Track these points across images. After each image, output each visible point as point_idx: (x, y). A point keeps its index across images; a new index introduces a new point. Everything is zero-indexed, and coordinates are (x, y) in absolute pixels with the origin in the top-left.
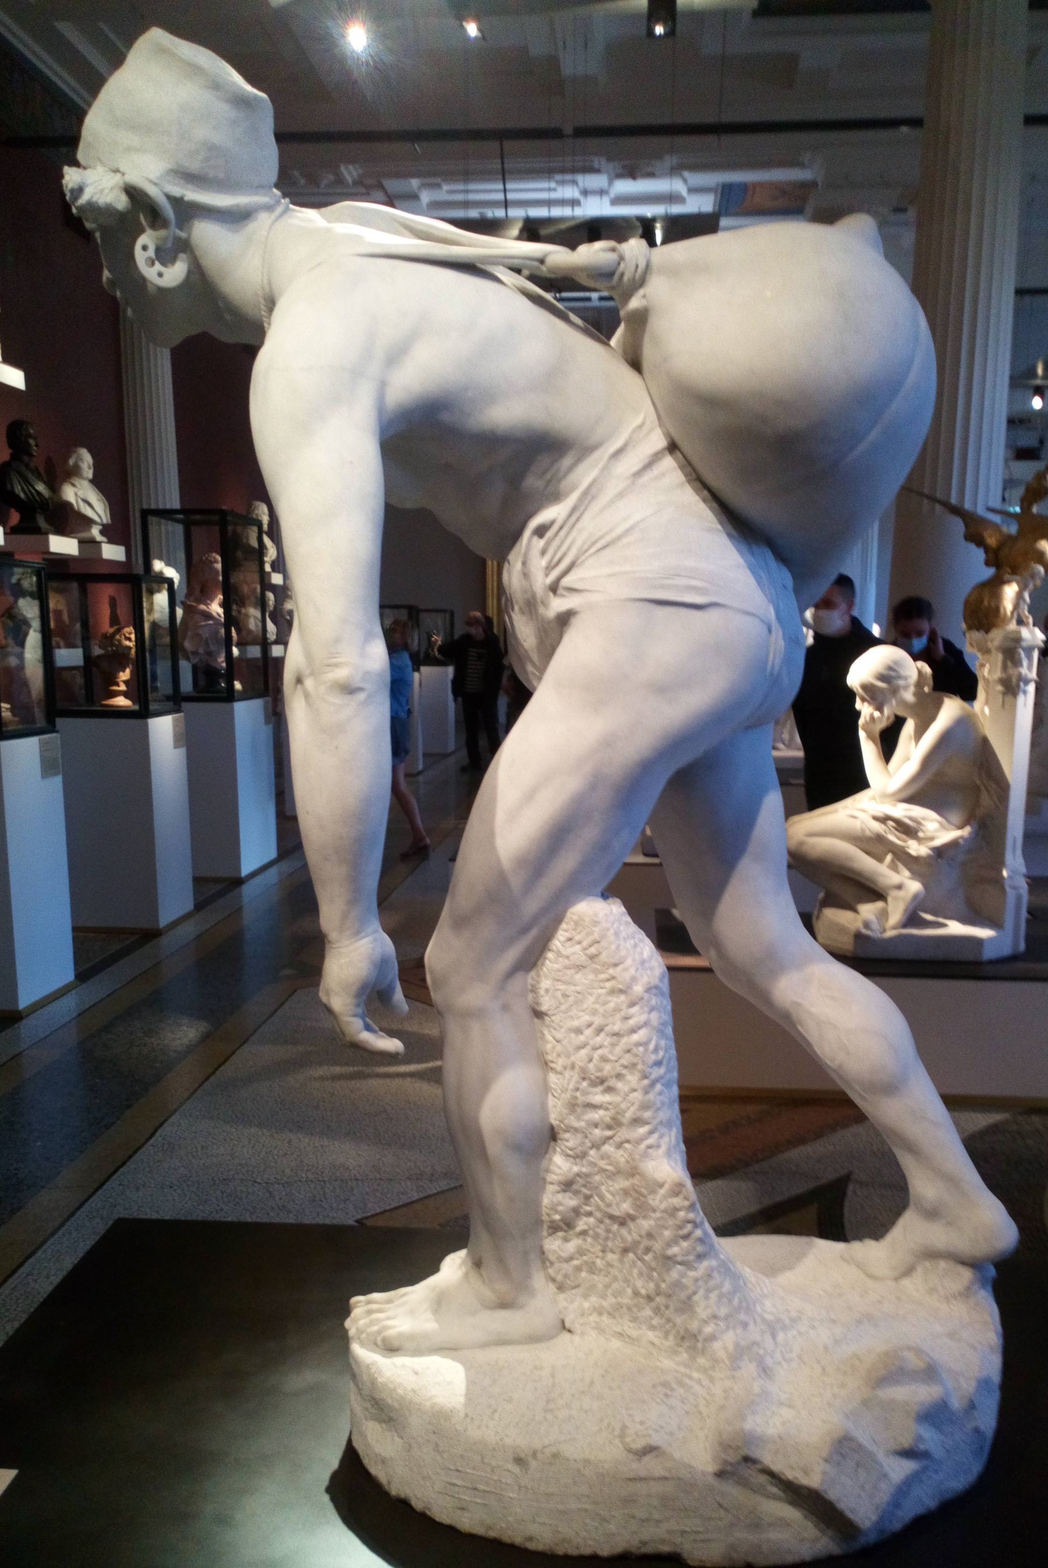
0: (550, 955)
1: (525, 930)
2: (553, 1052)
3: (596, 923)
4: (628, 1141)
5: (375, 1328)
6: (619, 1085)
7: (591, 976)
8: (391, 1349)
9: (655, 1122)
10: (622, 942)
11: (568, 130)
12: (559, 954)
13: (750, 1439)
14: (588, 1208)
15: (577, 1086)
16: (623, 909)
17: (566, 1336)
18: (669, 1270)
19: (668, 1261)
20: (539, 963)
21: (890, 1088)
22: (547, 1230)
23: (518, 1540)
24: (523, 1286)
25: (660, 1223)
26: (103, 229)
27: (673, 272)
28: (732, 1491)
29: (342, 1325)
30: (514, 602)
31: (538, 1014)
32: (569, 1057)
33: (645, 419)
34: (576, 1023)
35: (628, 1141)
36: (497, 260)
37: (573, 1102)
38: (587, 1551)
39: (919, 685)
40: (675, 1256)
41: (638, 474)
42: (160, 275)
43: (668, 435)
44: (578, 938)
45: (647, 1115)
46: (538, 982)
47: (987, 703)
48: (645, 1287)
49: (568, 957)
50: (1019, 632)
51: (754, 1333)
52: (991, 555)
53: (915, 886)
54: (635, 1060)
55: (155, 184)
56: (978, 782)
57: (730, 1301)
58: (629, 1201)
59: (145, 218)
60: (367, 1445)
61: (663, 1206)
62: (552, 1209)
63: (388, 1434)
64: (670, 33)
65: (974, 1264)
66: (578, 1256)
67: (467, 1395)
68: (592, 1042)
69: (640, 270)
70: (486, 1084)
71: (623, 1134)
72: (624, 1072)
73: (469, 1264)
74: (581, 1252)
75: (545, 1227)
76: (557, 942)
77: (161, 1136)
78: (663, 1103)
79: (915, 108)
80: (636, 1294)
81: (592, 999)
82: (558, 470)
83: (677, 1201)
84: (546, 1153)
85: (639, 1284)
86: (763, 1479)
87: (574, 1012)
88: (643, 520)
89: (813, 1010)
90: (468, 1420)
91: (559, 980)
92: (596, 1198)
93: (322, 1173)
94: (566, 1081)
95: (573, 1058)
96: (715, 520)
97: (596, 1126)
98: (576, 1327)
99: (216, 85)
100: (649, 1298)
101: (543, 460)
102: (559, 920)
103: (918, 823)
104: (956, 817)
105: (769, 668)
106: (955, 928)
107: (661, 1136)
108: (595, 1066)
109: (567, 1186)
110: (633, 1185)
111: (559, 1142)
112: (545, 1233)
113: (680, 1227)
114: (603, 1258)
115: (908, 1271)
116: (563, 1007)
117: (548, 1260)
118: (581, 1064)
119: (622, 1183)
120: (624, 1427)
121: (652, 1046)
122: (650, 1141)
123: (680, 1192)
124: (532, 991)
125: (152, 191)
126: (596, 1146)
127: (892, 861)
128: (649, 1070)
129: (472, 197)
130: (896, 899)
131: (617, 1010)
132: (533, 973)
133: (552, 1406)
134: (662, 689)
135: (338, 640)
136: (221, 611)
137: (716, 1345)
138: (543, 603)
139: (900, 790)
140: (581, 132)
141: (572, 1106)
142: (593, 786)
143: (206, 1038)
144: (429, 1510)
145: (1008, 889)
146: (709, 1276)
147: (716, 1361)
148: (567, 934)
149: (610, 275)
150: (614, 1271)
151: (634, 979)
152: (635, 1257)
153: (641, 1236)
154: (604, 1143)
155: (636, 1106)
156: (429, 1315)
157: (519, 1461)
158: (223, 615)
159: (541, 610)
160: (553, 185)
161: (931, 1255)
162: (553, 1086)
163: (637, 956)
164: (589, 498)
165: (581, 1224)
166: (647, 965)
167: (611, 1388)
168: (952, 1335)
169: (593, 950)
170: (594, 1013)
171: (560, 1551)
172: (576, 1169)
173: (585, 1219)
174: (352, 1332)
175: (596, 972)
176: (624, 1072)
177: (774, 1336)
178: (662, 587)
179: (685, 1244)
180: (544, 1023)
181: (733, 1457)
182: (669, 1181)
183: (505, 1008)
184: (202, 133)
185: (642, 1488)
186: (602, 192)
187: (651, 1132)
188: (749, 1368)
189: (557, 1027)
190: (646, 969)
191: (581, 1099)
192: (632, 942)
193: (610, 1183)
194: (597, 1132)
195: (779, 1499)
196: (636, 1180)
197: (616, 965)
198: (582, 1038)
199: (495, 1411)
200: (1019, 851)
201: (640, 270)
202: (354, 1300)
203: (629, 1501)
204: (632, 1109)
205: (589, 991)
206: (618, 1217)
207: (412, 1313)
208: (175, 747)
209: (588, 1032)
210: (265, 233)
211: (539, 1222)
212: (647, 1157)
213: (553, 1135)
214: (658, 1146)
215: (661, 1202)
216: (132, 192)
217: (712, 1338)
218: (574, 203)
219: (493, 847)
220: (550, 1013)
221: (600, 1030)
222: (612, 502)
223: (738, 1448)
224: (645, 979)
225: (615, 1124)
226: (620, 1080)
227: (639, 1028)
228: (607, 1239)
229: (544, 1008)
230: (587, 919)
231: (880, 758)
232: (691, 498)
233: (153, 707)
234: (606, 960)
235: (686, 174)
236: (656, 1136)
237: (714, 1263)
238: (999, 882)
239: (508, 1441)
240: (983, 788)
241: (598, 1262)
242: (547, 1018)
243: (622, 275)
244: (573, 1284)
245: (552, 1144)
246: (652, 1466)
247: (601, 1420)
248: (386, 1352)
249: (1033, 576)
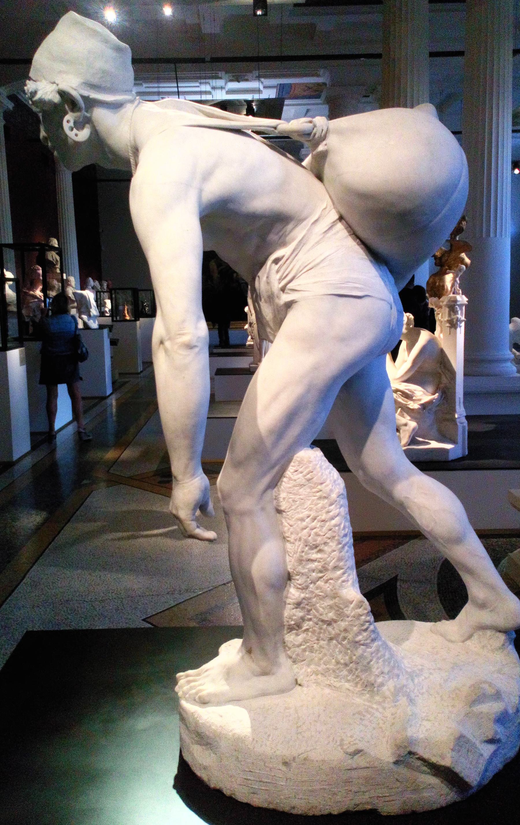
0: (285, 479)
1: (273, 467)
2: (288, 532)
3: (310, 462)
4: (331, 579)
5: (194, 691)
6: (326, 548)
7: (309, 490)
8: (204, 702)
9: (346, 567)
10: (323, 471)
11: (208, 59)
12: (290, 479)
13: (411, 741)
14: (309, 617)
15: (303, 550)
16: (322, 453)
17: (298, 688)
18: (357, 649)
19: (356, 644)
20: (279, 484)
21: (458, 540)
22: (287, 630)
23: (287, 809)
24: (274, 663)
25: (350, 623)
26: (44, 112)
27: (340, 132)
28: (403, 771)
29: (173, 690)
30: (262, 297)
31: (279, 511)
32: (298, 534)
33: (327, 205)
34: (301, 516)
35: (331, 579)
36: (247, 127)
37: (301, 558)
38: (326, 812)
39: (408, 324)
40: (360, 641)
41: (326, 232)
42: (76, 135)
43: (339, 212)
44: (300, 470)
45: (341, 564)
46: (279, 494)
47: (441, 332)
48: (342, 658)
49: (295, 480)
50: (455, 297)
51: (403, 680)
52: (438, 261)
53: (413, 424)
54: (334, 534)
55: (75, 90)
56: (440, 371)
57: (389, 663)
58: (333, 611)
59: (68, 107)
60: (194, 758)
61: (352, 614)
62: (290, 618)
63: (207, 753)
64: (265, 14)
65: (505, 632)
66: (304, 643)
67: (252, 727)
68: (310, 526)
69: (324, 132)
70: (254, 552)
71: (329, 575)
72: (328, 541)
73: (244, 651)
74: (305, 641)
75: (286, 628)
76: (289, 472)
77: (29, 578)
78: (349, 557)
79: (377, 49)
80: (338, 663)
81: (309, 502)
82: (286, 231)
83: (360, 611)
84: (285, 587)
85: (340, 657)
86: (419, 763)
87: (299, 510)
88: (330, 255)
89: (416, 500)
90: (255, 742)
91: (291, 493)
92: (314, 611)
93: (121, 594)
94: (296, 547)
95: (300, 535)
96: (364, 254)
97: (313, 571)
98: (304, 683)
99: (106, 41)
100: (346, 665)
101: (278, 226)
102: (290, 461)
103: (413, 392)
104: (431, 389)
105: (391, 327)
106: (434, 444)
107: (349, 575)
108: (312, 538)
109: (298, 605)
110: (335, 603)
111: (293, 581)
112: (285, 632)
113: (362, 625)
114: (318, 644)
115: (470, 637)
116: (293, 507)
117: (287, 646)
118: (305, 538)
119: (329, 602)
120: (342, 740)
121: (342, 526)
122: (344, 578)
123: (362, 606)
124: (275, 499)
125: (74, 93)
126: (313, 582)
127: (401, 412)
128: (341, 539)
129: (161, 90)
130: (404, 431)
131: (323, 508)
132: (276, 489)
133: (300, 730)
134: (343, 339)
135: (184, 321)
136: (41, 294)
137: (385, 688)
138: (278, 297)
139: (402, 376)
140: (214, 60)
141: (300, 561)
142: (308, 391)
143: (46, 521)
144: (234, 794)
145: (458, 424)
146: (378, 651)
147: (385, 698)
148: (295, 468)
149: (309, 134)
150: (324, 651)
151: (331, 491)
152: (337, 643)
153: (341, 631)
154: (318, 581)
155: (335, 559)
156: (223, 682)
157: (286, 763)
158: (43, 297)
159: (277, 301)
160: (198, 84)
161: (483, 628)
162: (289, 550)
163: (331, 478)
164: (302, 244)
165: (305, 626)
166: (337, 482)
167: (330, 717)
168: (499, 671)
169: (309, 476)
170: (311, 509)
171: (311, 813)
172: (303, 595)
173: (308, 623)
174: (180, 694)
175: (311, 488)
176: (328, 541)
177: (413, 680)
178: (341, 288)
179: (365, 634)
180: (282, 517)
181: (404, 752)
182: (356, 600)
183: (263, 509)
184: (100, 64)
185: (354, 774)
186: (222, 88)
187: (344, 573)
188: (403, 700)
189: (290, 518)
190: (337, 485)
191: (305, 557)
192: (328, 470)
193: (322, 602)
194: (314, 574)
195: (428, 773)
196: (336, 600)
197: (322, 484)
198: (304, 523)
199: (269, 736)
200: (462, 405)
201: (324, 132)
202: (179, 675)
203: (348, 782)
204: (333, 561)
205: (308, 498)
206: (327, 621)
207: (213, 681)
208: (21, 365)
209: (308, 520)
210: (131, 114)
211: (282, 626)
212: (343, 587)
213: (289, 577)
214: (348, 581)
215: (352, 612)
216: (62, 94)
217: (382, 685)
218: (209, 93)
219: (256, 425)
220: (286, 510)
221: (314, 519)
222: (313, 246)
223: (406, 747)
224: (337, 490)
225: (324, 569)
226: (326, 546)
227: (336, 517)
228: (320, 633)
229: (282, 508)
230: (306, 460)
231: (391, 360)
232: (352, 244)
233: (9, 345)
234: (316, 481)
235: (262, 80)
236: (346, 575)
237: (380, 643)
238: (454, 420)
239: (278, 753)
240: (442, 373)
241: (315, 645)
242: (284, 513)
243: (315, 134)
244: (302, 659)
245: (288, 582)
246: (360, 761)
247: (329, 737)
248: (202, 705)
249: (460, 270)
